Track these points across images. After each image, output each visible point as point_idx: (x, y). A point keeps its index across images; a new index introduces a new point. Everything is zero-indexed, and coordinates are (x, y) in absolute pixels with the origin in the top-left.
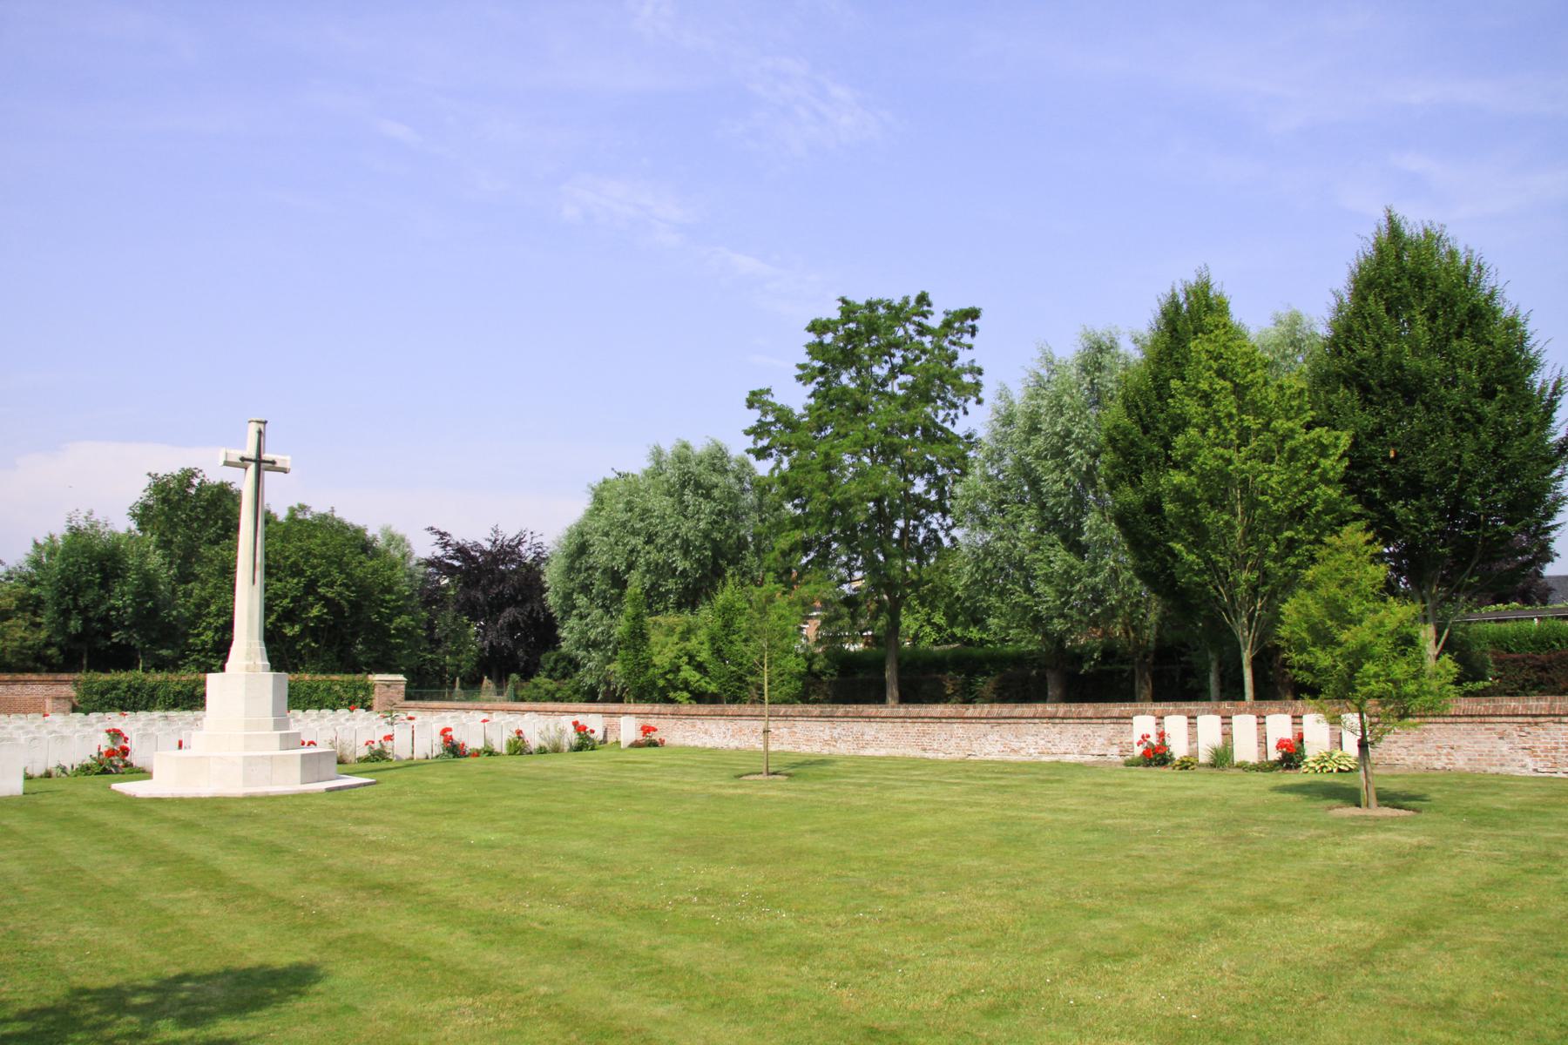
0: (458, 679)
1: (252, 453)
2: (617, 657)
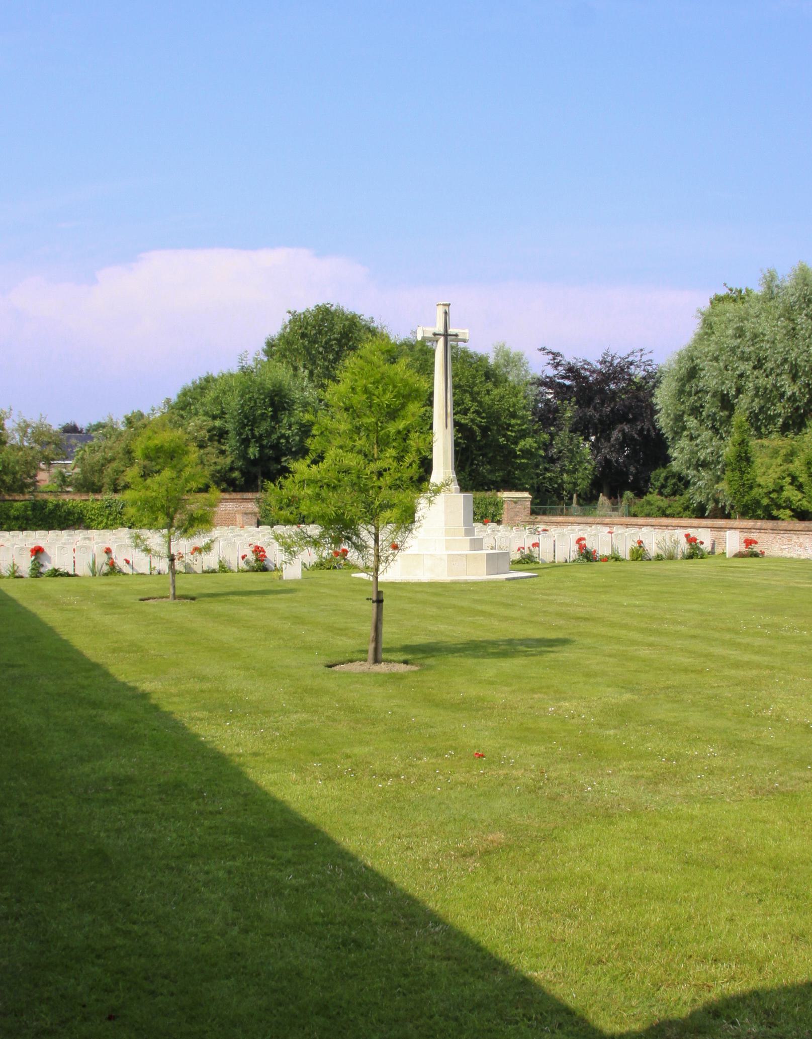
0: (575, 496)
1: (442, 331)
2: (725, 477)
